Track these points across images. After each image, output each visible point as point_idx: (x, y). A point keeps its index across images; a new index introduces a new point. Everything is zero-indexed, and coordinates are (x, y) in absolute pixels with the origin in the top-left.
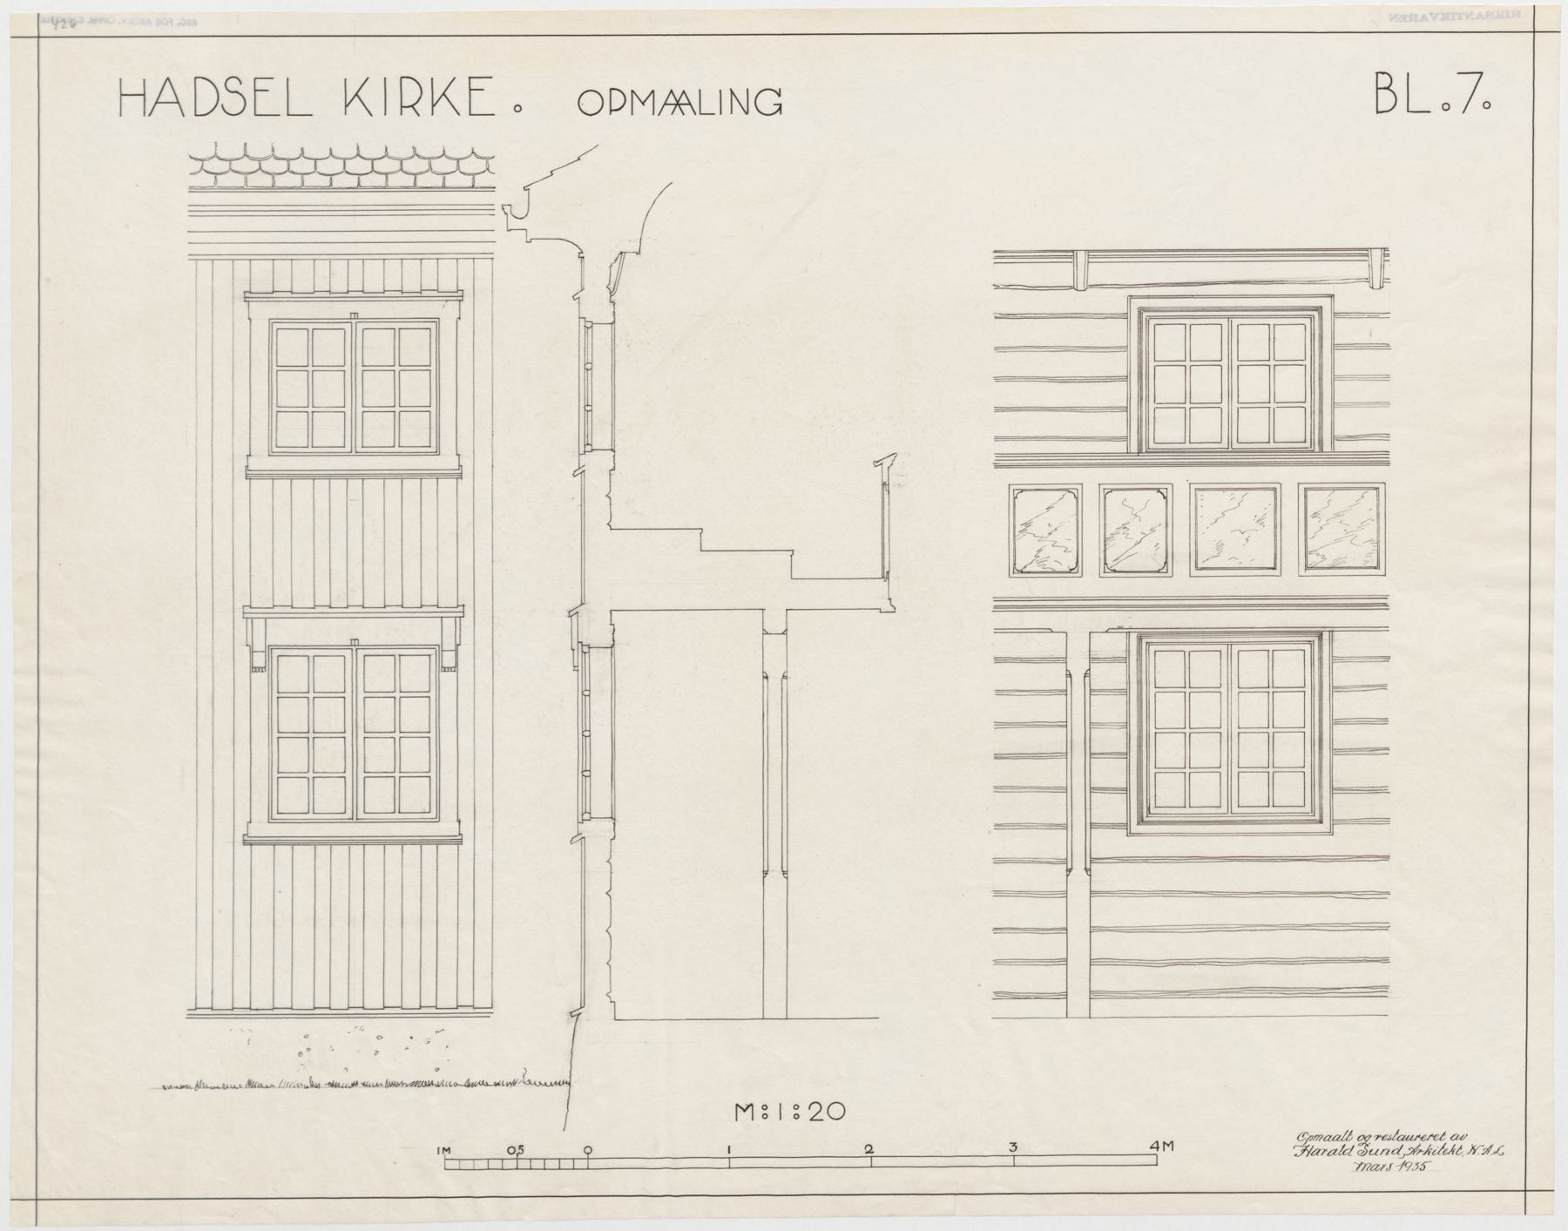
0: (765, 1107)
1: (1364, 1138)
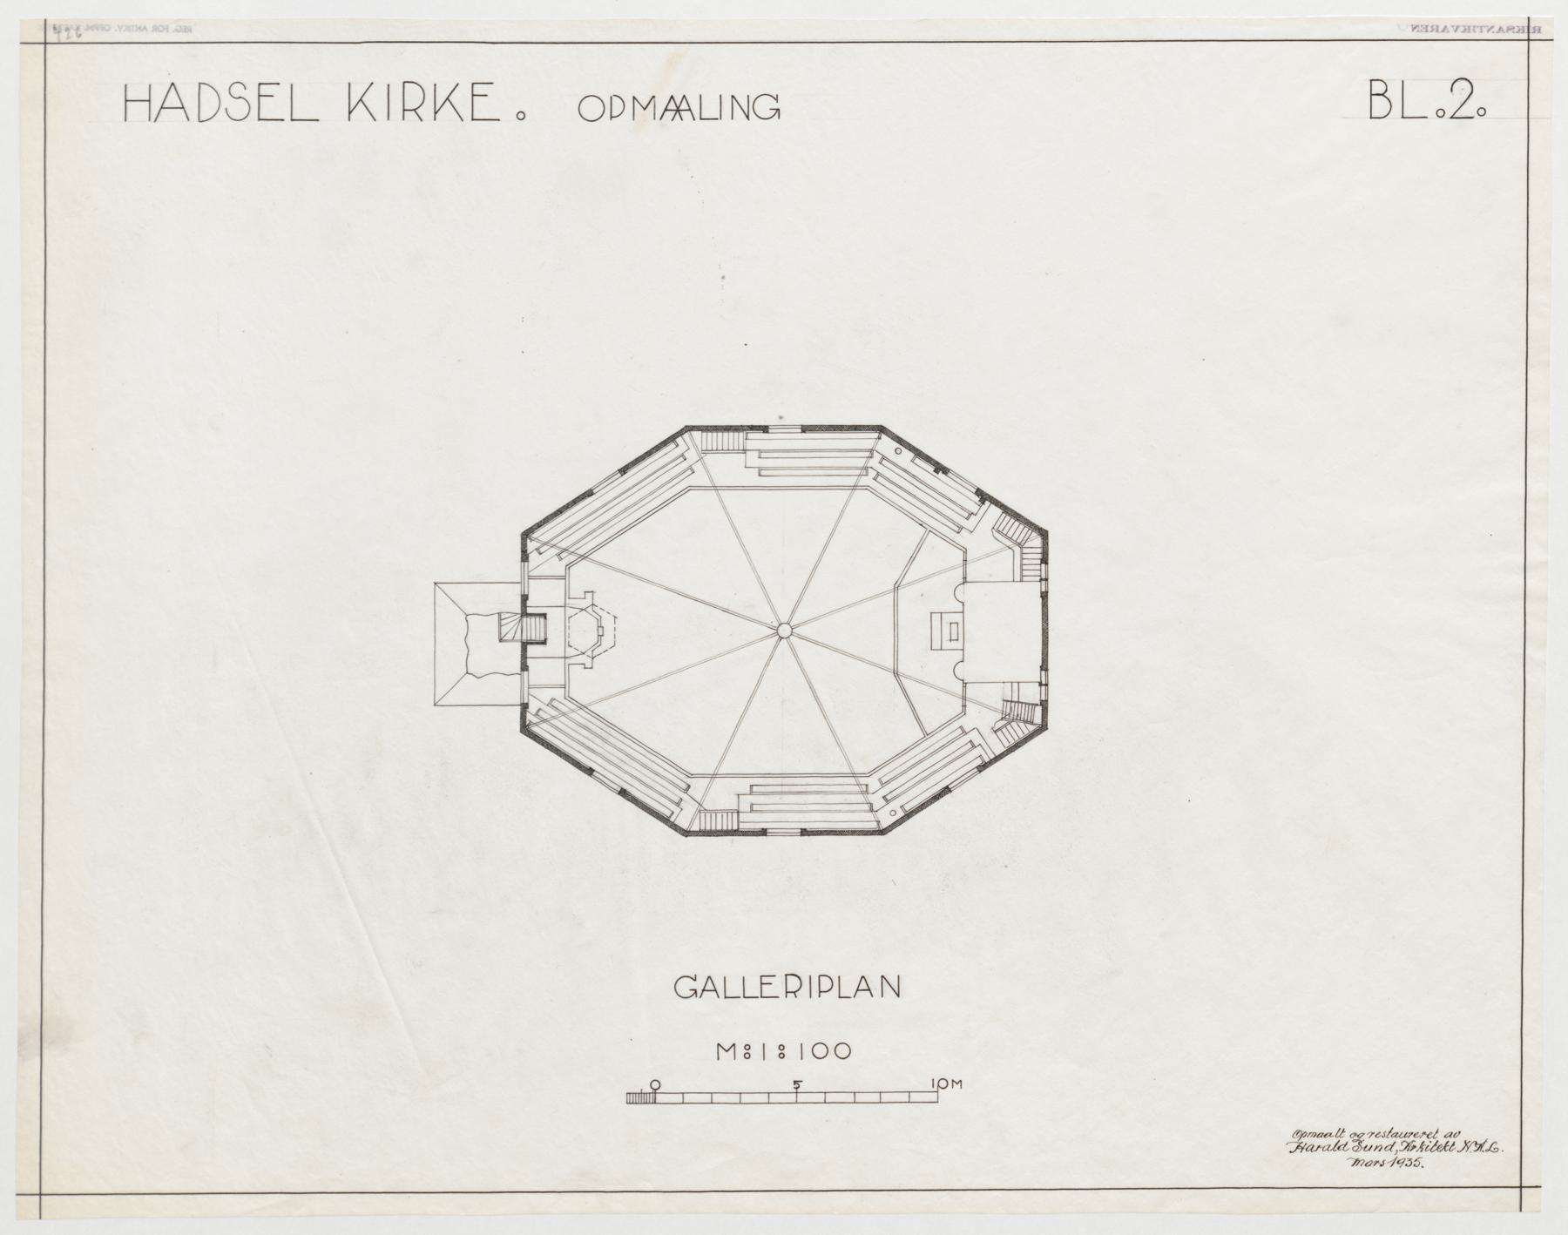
0: (747, 1047)
1: (1358, 1137)
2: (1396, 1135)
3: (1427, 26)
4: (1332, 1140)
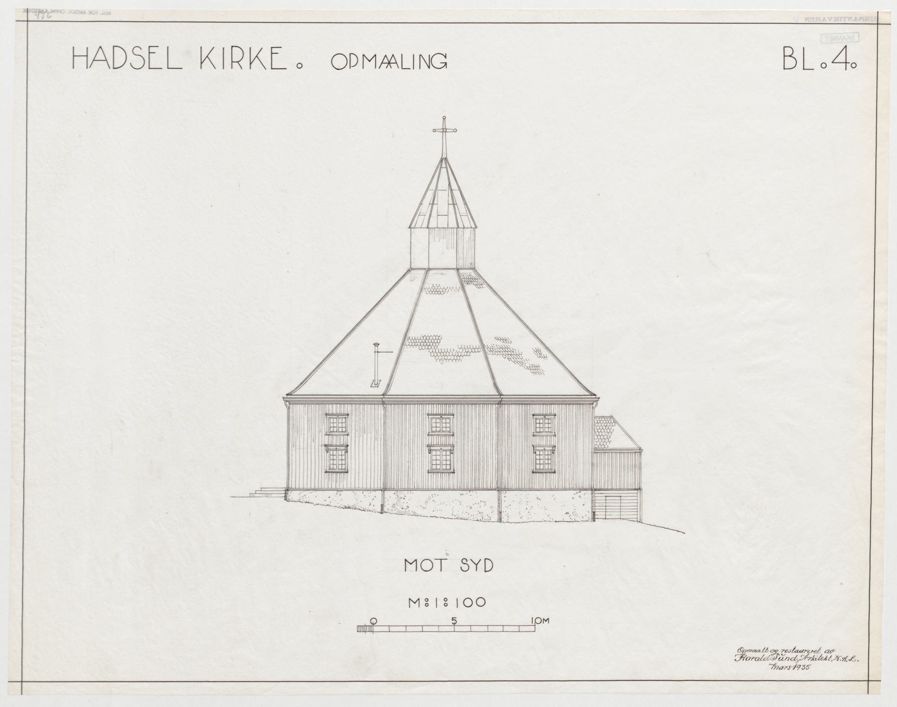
0: (427, 600)
2: (797, 651)
3: (814, 18)
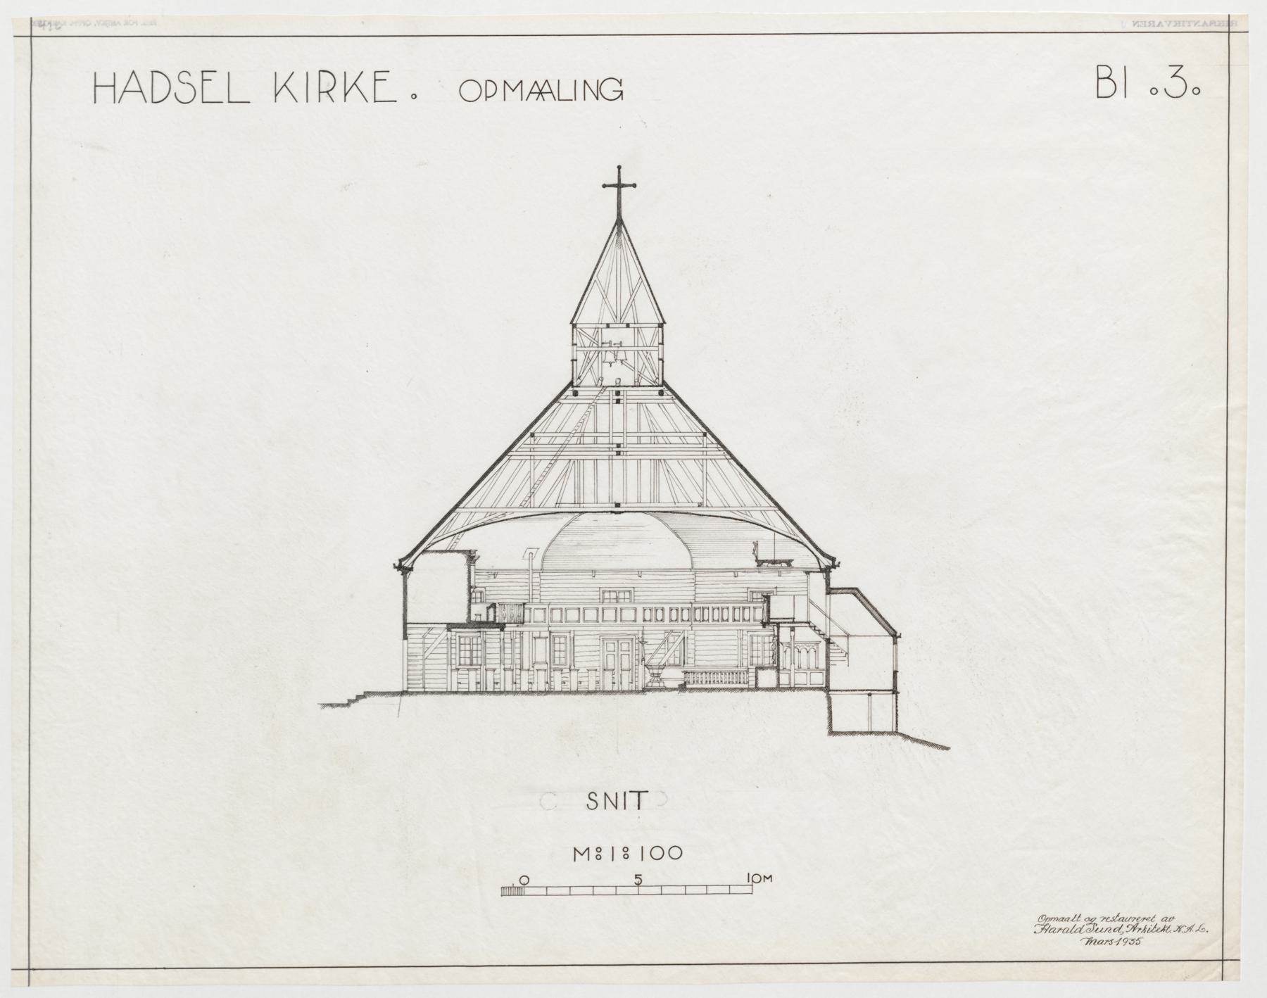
0: (599, 849)
1: (1091, 920)
4: (1070, 925)
